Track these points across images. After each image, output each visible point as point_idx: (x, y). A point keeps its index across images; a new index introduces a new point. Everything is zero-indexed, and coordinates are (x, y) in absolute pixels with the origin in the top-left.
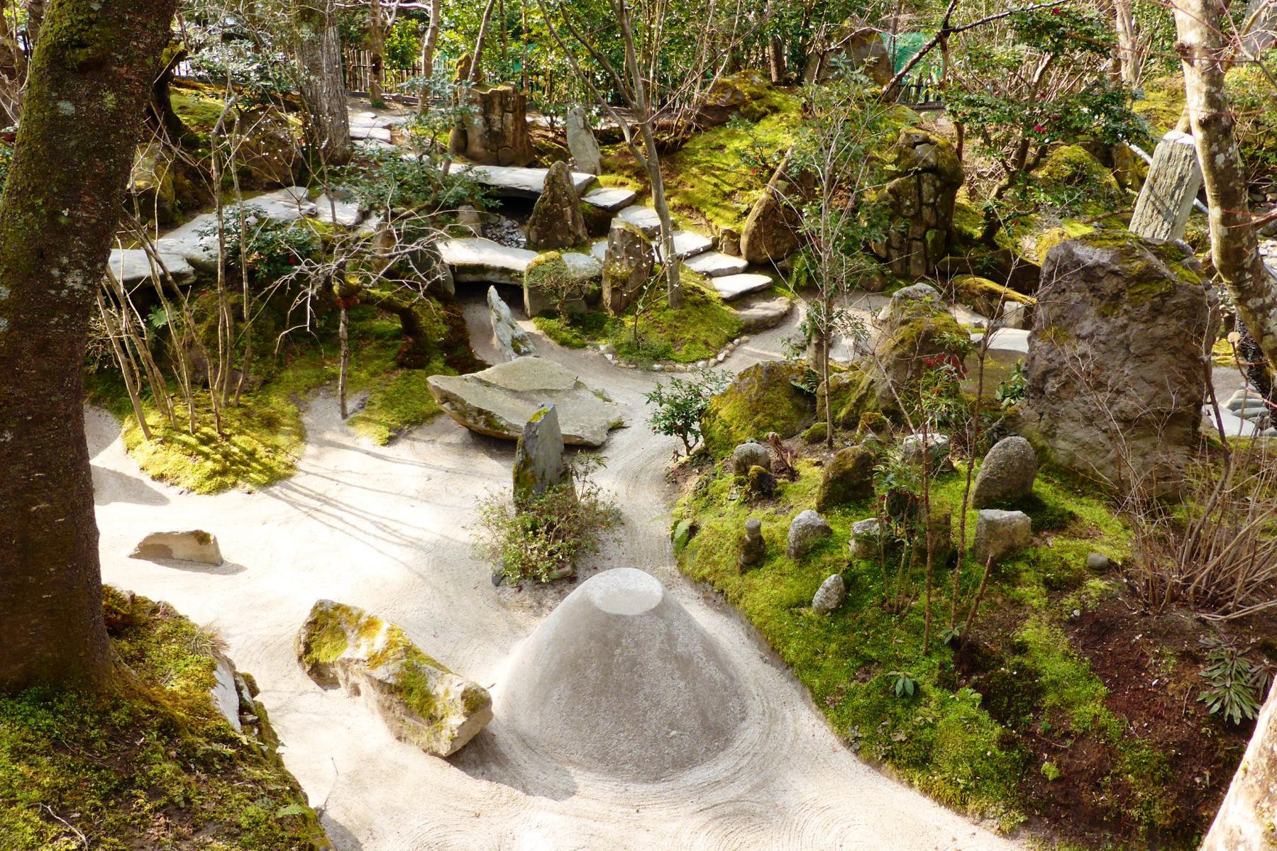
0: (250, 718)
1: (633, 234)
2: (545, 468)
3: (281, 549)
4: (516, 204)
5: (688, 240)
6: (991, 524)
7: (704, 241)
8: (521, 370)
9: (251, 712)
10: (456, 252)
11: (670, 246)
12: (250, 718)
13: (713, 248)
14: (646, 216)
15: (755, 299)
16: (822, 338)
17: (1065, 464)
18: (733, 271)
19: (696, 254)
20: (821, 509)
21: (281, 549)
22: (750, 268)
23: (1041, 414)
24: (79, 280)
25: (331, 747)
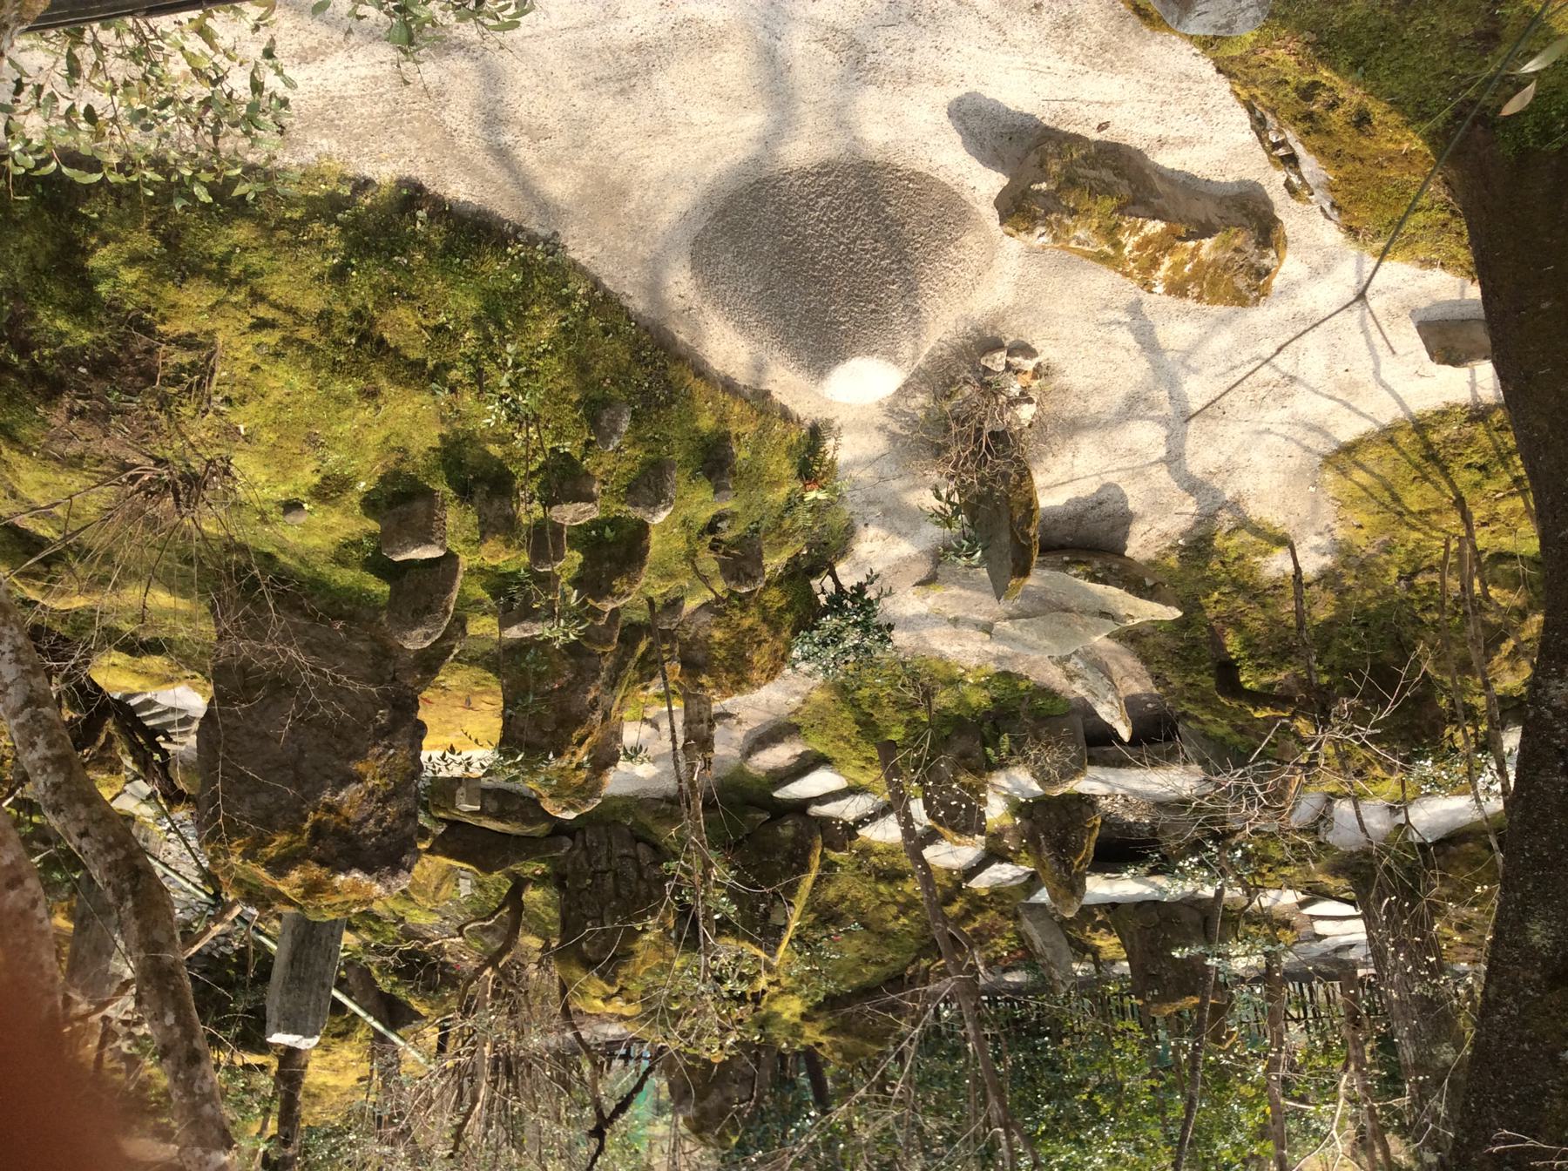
0: (1282, 152)
1: (953, 828)
2: (1003, 530)
3: (1295, 386)
4: (1120, 849)
5: (887, 833)
6: (425, 539)
7: (869, 833)
8: (1090, 654)
9: (1282, 158)
10: (1176, 780)
11: (907, 822)
12: (1282, 152)
13: (861, 822)
14: (950, 854)
15: (788, 768)
16: (699, 739)
17: (1470, 400)
18: (822, 800)
19: (873, 818)
20: (643, 528)
21: (1295, 386)
22: (801, 806)
23: (394, 679)
24: (1553, 692)
25: (1189, 117)
